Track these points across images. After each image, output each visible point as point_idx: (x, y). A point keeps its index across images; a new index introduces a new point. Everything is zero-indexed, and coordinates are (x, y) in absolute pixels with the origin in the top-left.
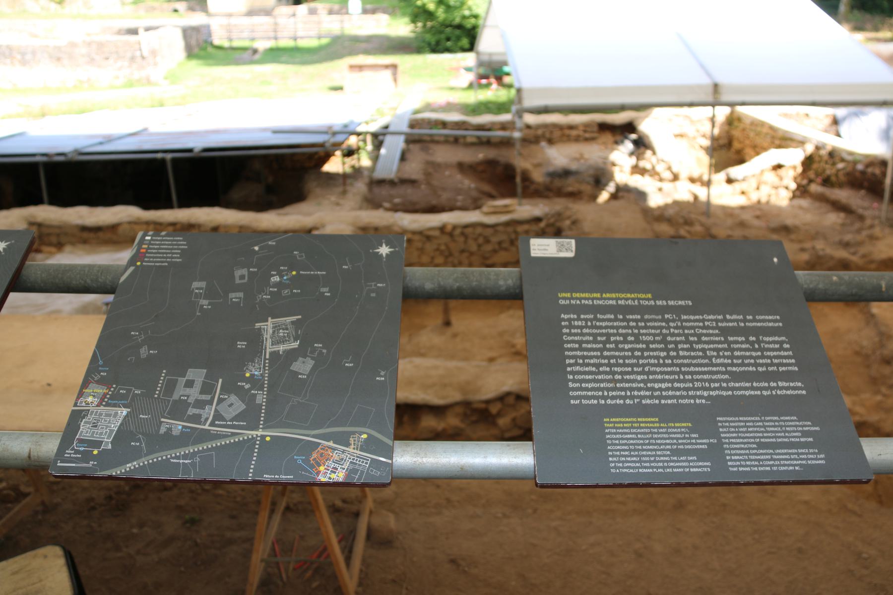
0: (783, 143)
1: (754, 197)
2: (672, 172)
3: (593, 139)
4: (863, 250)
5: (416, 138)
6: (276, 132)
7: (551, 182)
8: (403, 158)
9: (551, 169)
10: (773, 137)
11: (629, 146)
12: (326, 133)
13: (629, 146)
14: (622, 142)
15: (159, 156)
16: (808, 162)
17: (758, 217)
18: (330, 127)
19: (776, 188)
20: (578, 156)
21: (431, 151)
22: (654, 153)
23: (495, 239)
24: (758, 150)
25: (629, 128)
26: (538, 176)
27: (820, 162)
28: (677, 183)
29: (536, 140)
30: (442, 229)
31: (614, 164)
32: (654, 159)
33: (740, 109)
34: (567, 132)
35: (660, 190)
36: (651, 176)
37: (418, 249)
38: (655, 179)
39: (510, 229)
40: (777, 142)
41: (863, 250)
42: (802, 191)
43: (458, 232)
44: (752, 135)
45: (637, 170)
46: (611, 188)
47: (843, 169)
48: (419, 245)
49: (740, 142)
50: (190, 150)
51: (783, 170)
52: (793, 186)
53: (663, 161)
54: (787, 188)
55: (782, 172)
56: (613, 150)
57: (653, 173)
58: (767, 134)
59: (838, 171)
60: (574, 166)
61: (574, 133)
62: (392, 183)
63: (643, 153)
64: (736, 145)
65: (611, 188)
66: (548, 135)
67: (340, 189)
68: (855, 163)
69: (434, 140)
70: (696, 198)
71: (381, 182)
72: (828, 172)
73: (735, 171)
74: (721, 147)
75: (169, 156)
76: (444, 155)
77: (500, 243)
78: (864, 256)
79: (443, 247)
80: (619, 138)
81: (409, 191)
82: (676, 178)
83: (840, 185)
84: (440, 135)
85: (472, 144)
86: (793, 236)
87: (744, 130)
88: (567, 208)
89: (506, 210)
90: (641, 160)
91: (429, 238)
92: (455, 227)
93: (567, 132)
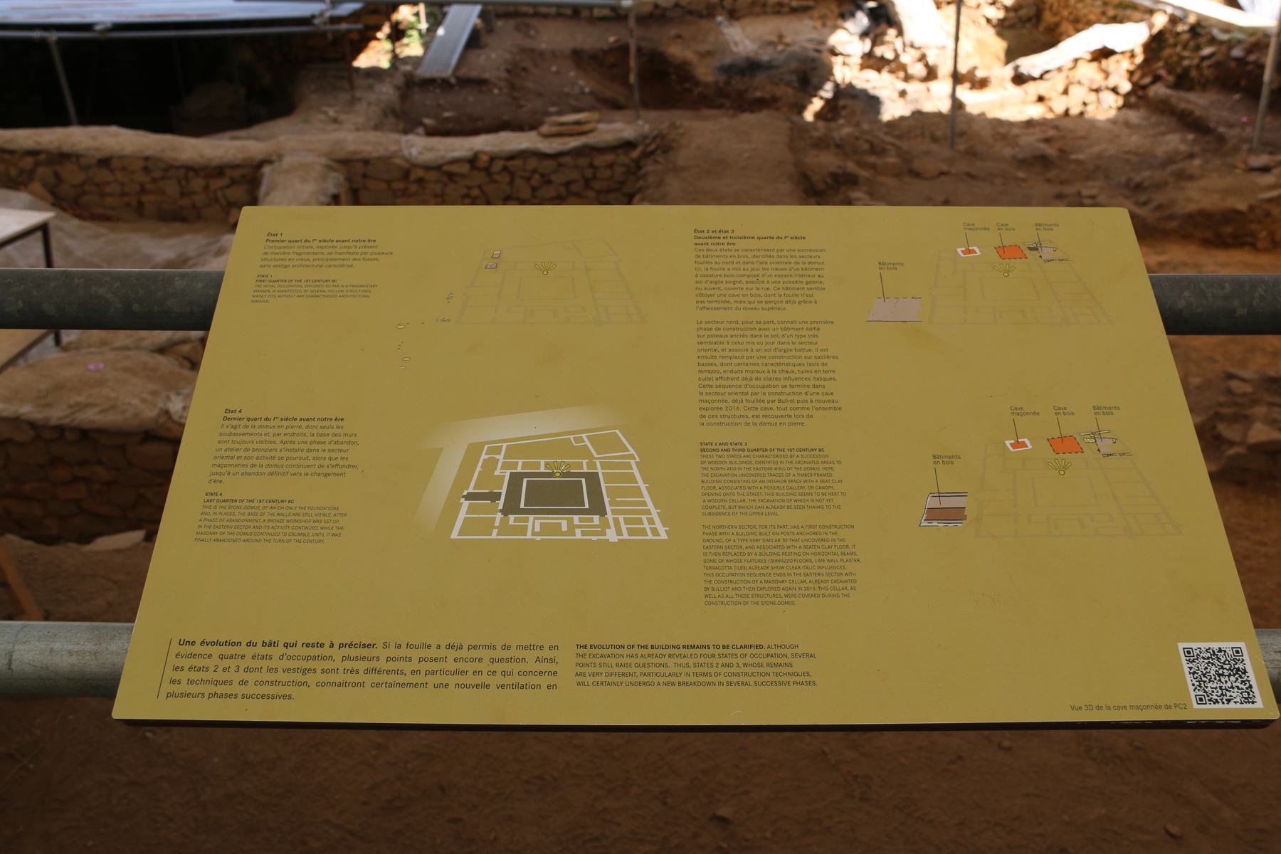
0: (1121, 13)
1: (1059, 106)
2: (927, 65)
4: (1160, 198)
5: (511, 9)
7: (728, 83)
8: (474, 41)
9: (728, 60)
11: (862, 20)
13: (862, 20)
14: (853, 15)
15: (36, 34)
16: (1155, 44)
19: (1097, 91)
20: (774, 39)
21: (532, 33)
22: (900, 33)
23: (558, 178)
24: (1080, 24)
26: (705, 73)
27: (1175, 45)
28: (933, 85)
30: (473, 161)
31: (834, 53)
32: (898, 43)
35: (903, 94)
36: (892, 72)
38: (897, 78)
39: (583, 162)
40: (1111, 12)
41: (1160, 198)
42: (1136, 98)
43: (498, 166)
45: (872, 62)
46: (827, 91)
50: (87, 27)
51: (1113, 59)
52: (1126, 87)
53: (912, 46)
54: (1114, 90)
55: (1110, 63)
56: (836, 28)
57: (894, 66)
59: (1204, 58)
60: (765, 57)
62: (444, 84)
63: (884, 34)
64: (1048, 18)
65: (827, 91)
67: (346, 96)
68: (1230, 44)
71: (428, 83)
72: (1186, 63)
73: (1031, 64)
74: (1024, 21)
75: (53, 36)
76: (553, 37)
78: (1160, 207)
80: (847, 7)
81: (471, 98)
82: (931, 74)
83: (1204, 85)
85: (603, 19)
86: (1052, 174)
88: (673, 126)
89: (578, 129)
90: (879, 46)
91: (451, 176)
92: (493, 158)
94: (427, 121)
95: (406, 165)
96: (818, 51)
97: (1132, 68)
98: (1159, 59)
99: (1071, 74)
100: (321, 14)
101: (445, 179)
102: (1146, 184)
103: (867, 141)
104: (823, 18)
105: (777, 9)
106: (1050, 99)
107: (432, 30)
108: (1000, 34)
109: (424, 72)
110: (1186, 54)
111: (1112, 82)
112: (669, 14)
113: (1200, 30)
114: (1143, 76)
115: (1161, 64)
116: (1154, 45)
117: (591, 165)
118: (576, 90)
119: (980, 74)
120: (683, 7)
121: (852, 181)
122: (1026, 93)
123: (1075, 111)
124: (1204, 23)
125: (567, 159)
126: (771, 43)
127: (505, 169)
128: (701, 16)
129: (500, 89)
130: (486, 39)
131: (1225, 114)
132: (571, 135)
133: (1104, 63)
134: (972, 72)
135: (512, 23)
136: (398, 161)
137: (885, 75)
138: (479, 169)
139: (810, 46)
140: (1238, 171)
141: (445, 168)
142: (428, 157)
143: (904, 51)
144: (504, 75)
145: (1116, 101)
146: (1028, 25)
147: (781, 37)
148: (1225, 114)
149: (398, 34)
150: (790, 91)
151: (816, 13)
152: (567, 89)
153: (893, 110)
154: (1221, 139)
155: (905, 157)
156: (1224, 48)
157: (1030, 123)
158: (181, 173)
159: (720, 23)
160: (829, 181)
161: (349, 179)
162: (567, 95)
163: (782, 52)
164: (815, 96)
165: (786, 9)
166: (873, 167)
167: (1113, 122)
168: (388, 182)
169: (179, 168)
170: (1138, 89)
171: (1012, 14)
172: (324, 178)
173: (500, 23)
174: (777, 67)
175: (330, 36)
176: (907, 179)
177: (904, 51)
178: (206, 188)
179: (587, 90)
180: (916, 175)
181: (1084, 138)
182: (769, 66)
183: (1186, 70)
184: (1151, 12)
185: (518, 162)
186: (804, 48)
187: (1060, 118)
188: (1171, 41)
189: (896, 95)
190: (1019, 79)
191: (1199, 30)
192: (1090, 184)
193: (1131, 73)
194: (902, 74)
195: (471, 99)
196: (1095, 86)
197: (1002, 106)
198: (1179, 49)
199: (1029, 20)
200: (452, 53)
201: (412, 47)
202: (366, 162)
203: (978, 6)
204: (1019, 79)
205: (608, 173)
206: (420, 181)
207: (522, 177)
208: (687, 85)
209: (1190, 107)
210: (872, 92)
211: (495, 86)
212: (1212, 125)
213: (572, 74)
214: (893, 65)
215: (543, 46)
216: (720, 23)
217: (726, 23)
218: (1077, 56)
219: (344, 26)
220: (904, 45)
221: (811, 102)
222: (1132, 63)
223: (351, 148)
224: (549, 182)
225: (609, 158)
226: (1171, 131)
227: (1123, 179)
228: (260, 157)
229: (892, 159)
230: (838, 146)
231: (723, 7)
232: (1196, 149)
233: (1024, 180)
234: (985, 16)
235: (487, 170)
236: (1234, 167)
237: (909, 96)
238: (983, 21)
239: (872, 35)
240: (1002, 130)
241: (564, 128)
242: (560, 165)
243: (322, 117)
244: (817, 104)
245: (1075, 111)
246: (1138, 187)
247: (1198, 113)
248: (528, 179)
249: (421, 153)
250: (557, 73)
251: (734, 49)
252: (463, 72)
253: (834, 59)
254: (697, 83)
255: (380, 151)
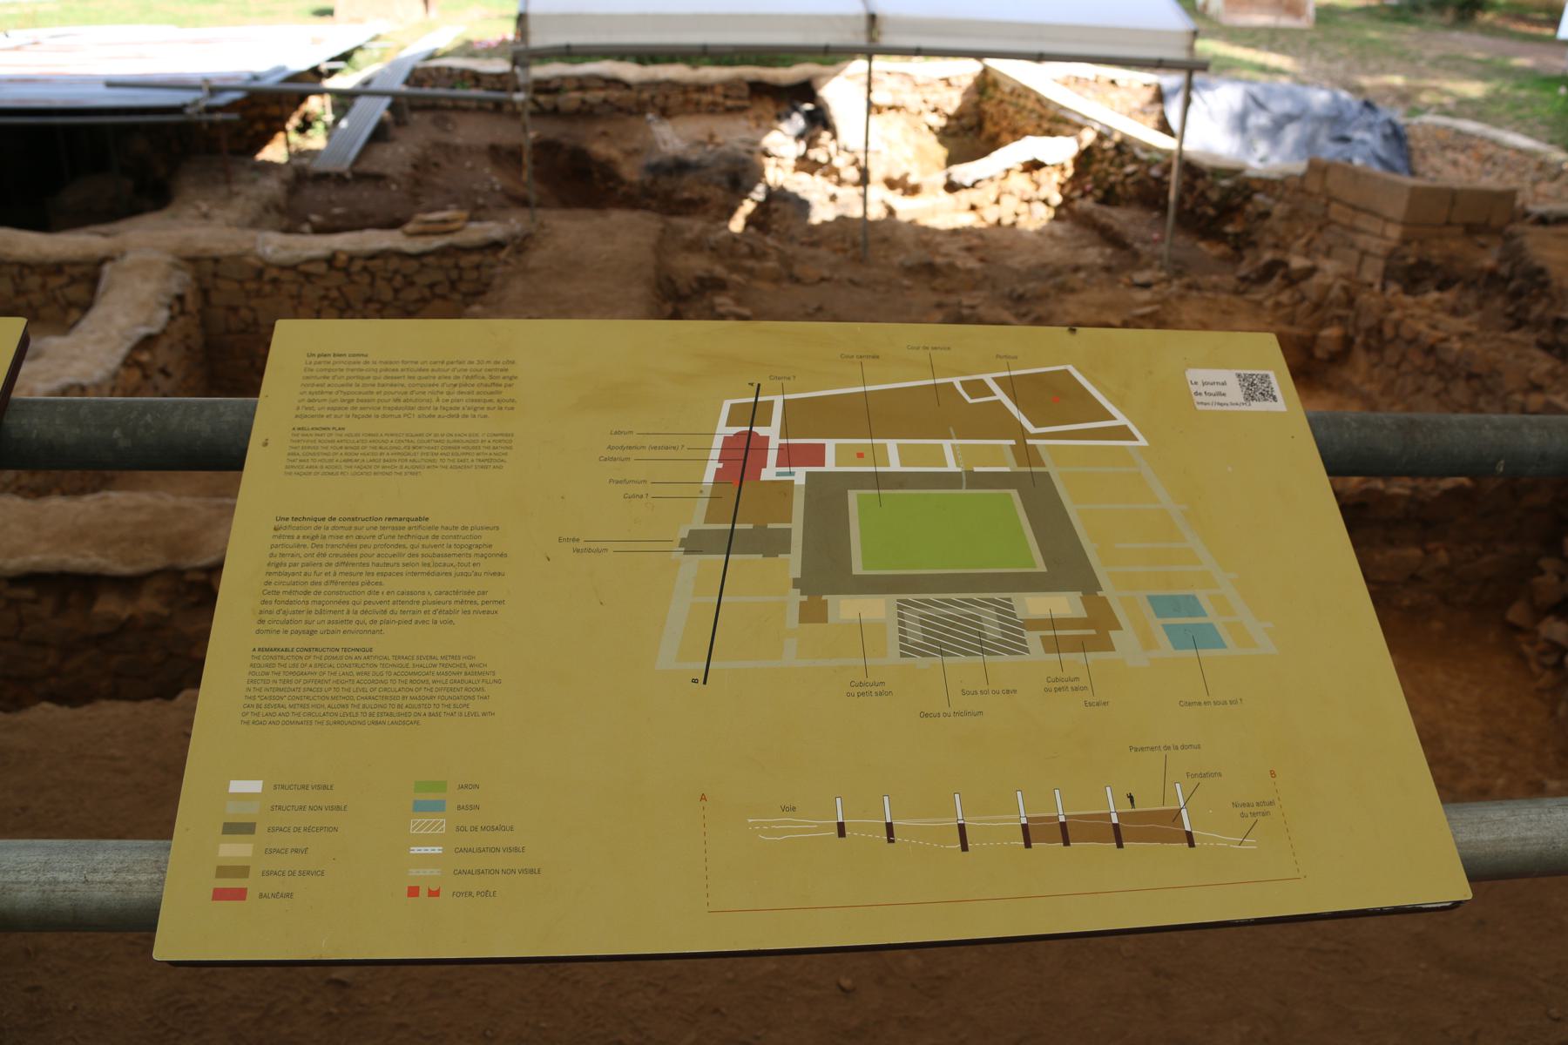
0: (1054, 126)
1: (991, 215)
3: (741, 110)
6: (111, 84)
7: (654, 182)
8: (380, 134)
9: (654, 159)
10: (1041, 117)
11: (798, 122)
12: (197, 88)
13: (798, 122)
14: (788, 116)
16: (1085, 159)
17: (969, 249)
18: (206, 81)
19: (1029, 201)
20: (704, 138)
21: (450, 126)
22: (835, 137)
23: (422, 280)
24: (1017, 134)
25: (805, 91)
26: (631, 172)
27: (1102, 161)
29: (640, 109)
30: (331, 260)
31: (766, 154)
32: (832, 146)
33: (996, 65)
34: (695, 96)
35: (833, 198)
36: (825, 175)
37: (292, 297)
38: (831, 181)
39: (448, 262)
40: (1046, 125)
42: (1065, 212)
44: (1011, 110)
45: (806, 164)
46: (759, 194)
47: (1133, 174)
48: (294, 289)
49: (996, 124)
51: (1043, 171)
52: (1057, 199)
54: (1046, 202)
55: (1040, 175)
56: (770, 129)
58: (1032, 111)
59: (1128, 176)
60: (693, 157)
61: (706, 98)
62: (339, 179)
63: (818, 136)
64: (990, 128)
65: (759, 194)
66: (659, 100)
67: (223, 190)
68: (1150, 164)
69: (458, 107)
70: (891, 212)
71: (322, 178)
72: (1112, 179)
73: (965, 172)
76: (472, 132)
77: (432, 286)
79: (334, 294)
80: (785, 108)
84: (469, 99)
86: (938, 282)
87: (1001, 102)
89: (444, 228)
90: (812, 148)
91: (308, 276)
92: (352, 258)
93: (695, 96)
94: (315, 218)
95: (259, 264)
96: (750, 152)
97: (1062, 181)
98: (1088, 174)
99: (1004, 183)
100: (196, 103)
101: (302, 279)
102: (1028, 295)
103: (748, 244)
104: (758, 118)
105: (711, 107)
106: (982, 208)
107: (336, 122)
108: (941, 142)
109: (319, 166)
110: (1112, 170)
111: (1043, 194)
112: (597, 110)
113: (1123, 147)
114: (1073, 189)
115: (1090, 178)
116: (1084, 160)
117: (457, 266)
118: (487, 187)
119: (912, 180)
120: (611, 104)
121: (720, 285)
122: (958, 200)
123: (1007, 221)
124: (1128, 142)
125: (430, 260)
126: (701, 143)
127: (365, 269)
128: (630, 113)
129: (399, 184)
130: (394, 132)
131: (1143, 230)
132: (436, 233)
133: (1036, 174)
134: (904, 178)
135: (428, 116)
136: (251, 260)
137: (818, 178)
138: (338, 269)
139: (742, 147)
140: (1121, 286)
141: (302, 268)
142: (283, 256)
143: (838, 154)
144: (408, 170)
145: (1048, 213)
146: (971, 134)
147: (712, 137)
148: (1143, 230)
149: (305, 126)
150: (720, 193)
151: (751, 114)
152: (476, 186)
153: (821, 213)
154: (1136, 255)
155: (787, 261)
156: (1144, 168)
157: (955, 232)
158: (15, 270)
159: (650, 121)
160: (695, 285)
161: (198, 279)
162: (476, 193)
163: (711, 152)
164: (747, 198)
165: (721, 109)
166: (750, 272)
167: (1039, 233)
168: (241, 282)
169: (12, 264)
170: (1067, 200)
171: (954, 123)
172: (168, 277)
173: (416, 116)
174: (706, 167)
175: (205, 126)
176: (786, 285)
177: (838, 154)
178: (43, 286)
179: (498, 187)
180: (797, 280)
181: (1007, 248)
182: (697, 167)
183: (1112, 186)
184: (1080, 127)
185: (377, 263)
186: (735, 149)
187: (991, 227)
188: (1099, 156)
189: (826, 199)
190: (951, 187)
191: (1124, 148)
192: (975, 293)
193: (1062, 186)
194: (834, 178)
195: (366, 195)
196: (1026, 197)
197: (934, 213)
198: (1105, 165)
199: (971, 129)
200: (352, 146)
201: (316, 140)
202: (216, 260)
203: (920, 113)
204: (951, 187)
205: (475, 275)
206: (275, 281)
207: (384, 279)
208: (611, 184)
209: (1111, 222)
210: (803, 195)
211: (394, 181)
212: (1129, 241)
213: (487, 170)
214: (826, 169)
215: (459, 141)
216: (650, 121)
217: (656, 121)
218: (1008, 166)
219: (219, 116)
220: (838, 148)
221: (742, 204)
222: (1063, 176)
223: (201, 245)
224: (412, 284)
225: (476, 258)
226: (1092, 245)
227: (1007, 290)
228: (101, 253)
229: (771, 264)
230: (713, 249)
231: (654, 105)
232: (1114, 263)
233: (908, 288)
234: (926, 123)
235: (346, 271)
236: (1119, 282)
237: (839, 201)
238: (925, 128)
239: (807, 137)
240: (926, 237)
241: (430, 227)
242: (423, 265)
243: (192, 212)
244: (748, 207)
245: (1007, 221)
246: (1021, 298)
247: (1117, 227)
248: (390, 280)
249: (275, 251)
250: (472, 169)
251: (662, 147)
252: (365, 166)
253: (766, 161)
254: (622, 182)
255: (232, 249)
